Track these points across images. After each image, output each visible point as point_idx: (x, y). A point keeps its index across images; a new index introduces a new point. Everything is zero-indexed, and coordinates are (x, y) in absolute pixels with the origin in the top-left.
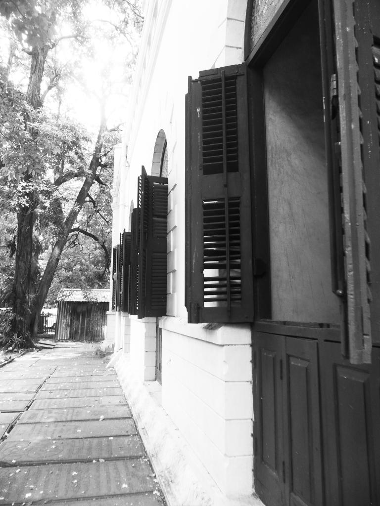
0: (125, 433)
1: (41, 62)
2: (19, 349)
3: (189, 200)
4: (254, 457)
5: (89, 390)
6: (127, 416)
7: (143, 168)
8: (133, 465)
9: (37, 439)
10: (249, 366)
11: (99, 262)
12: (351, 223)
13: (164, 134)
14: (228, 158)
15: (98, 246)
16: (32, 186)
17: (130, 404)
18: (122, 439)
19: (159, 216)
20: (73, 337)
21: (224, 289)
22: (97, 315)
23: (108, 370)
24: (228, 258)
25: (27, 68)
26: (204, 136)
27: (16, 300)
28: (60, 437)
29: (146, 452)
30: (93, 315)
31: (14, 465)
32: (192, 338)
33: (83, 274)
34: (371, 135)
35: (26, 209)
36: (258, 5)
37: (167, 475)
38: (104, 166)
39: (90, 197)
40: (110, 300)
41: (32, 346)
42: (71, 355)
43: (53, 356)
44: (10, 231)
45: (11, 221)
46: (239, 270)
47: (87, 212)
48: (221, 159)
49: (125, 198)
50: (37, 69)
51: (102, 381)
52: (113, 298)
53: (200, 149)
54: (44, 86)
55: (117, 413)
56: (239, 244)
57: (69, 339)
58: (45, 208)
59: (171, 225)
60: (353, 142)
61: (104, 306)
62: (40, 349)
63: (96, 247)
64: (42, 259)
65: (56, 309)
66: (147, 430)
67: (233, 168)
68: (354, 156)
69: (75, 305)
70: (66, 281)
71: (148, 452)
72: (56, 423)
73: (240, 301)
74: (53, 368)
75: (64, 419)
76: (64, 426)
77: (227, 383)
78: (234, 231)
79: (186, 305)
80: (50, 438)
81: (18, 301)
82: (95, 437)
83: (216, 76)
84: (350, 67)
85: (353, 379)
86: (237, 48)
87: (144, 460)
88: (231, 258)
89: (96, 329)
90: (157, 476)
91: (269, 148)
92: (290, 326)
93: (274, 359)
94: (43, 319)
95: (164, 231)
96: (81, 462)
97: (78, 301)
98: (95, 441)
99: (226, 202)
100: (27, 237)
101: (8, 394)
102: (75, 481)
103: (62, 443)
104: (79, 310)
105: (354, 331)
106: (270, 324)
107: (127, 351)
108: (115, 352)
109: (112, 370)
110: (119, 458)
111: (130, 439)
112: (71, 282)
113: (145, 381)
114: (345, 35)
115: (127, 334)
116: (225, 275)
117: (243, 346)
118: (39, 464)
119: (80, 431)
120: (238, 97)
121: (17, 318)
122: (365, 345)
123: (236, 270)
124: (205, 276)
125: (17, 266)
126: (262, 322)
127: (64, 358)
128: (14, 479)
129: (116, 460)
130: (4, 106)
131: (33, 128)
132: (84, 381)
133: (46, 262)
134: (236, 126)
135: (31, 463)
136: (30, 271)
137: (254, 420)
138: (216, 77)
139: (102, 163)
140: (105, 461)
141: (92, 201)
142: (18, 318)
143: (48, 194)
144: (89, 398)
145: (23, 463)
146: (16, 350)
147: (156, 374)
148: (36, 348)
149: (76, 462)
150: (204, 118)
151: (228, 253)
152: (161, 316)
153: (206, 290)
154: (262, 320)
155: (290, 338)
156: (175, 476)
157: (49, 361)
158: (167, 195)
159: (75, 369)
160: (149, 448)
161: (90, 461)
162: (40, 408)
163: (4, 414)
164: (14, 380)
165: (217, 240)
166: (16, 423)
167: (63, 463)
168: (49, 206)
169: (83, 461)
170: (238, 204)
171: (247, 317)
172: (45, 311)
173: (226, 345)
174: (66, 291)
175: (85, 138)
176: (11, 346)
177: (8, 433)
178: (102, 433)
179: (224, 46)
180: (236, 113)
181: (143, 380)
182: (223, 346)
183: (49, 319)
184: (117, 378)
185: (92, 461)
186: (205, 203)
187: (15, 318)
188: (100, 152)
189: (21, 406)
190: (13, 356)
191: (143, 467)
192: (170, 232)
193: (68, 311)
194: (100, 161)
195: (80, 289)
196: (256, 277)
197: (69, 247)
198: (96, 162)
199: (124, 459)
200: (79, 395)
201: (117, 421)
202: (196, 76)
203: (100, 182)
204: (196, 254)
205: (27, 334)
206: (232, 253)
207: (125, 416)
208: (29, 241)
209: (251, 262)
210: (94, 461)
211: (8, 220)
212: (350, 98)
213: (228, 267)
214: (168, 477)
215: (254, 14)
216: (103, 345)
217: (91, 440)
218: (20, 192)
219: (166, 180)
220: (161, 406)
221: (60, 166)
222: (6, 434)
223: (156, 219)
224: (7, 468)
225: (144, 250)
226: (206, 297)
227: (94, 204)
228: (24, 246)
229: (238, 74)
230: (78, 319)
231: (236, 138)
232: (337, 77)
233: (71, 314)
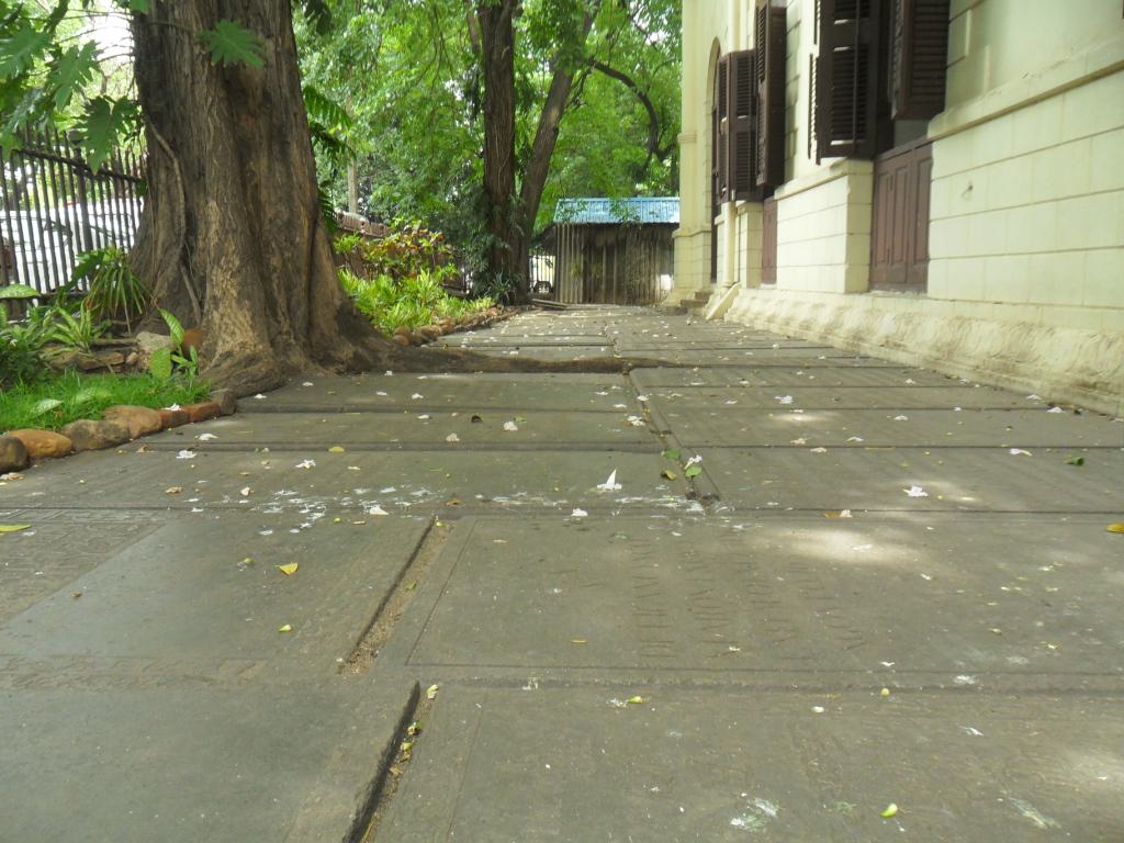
22: (638, 253)
27: (492, 207)
30: (630, 253)
69: (591, 234)
81: (497, 209)
104: (600, 241)
121: (497, 244)
124: (134, 207)
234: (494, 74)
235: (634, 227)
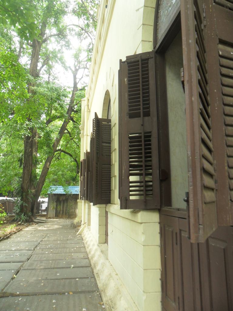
0: (86, 276)
1: (38, 51)
2: (25, 223)
3: (120, 134)
4: (161, 293)
5: (65, 249)
6: (88, 265)
7: (96, 113)
8: (90, 296)
9: (32, 279)
10: (158, 237)
11: (73, 170)
12: (192, 157)
13: (109, 92)
14: (144, 108)
15: (72, 160)
16: (31, 124)
17: (90, 258)
18: (84, 280)
19: (106, 143)
20: (57, 215)
21: (142, 188)
23: (78, 236)
24: (144, 169)
25: (30, 54)
26: (129, 95)
27: (23, 193)
28: (47, 278)
29: (98, 288)
30: (69, 202)
31: (18, 295)
32: (125, 218)
33: (63, 177)
34: (217, 98)
35: (28, 138)
36: (160, 16)
37: (110, 303)
38: (76, 112)
39: (68, 131)
40: (79, 193)
41: (32, 221)
42: (56, 227)
43: (45, 227)
44: (19, 152)
45: (20, 146)
46: (151, 177)
47: (66, 140)
48: (140, 109)
49: (88, 130)
50: (35, 57)
51: (73, 243)
52: (81, 192)
53: (127, 103)
54: (40, 65)
55: (82, 263)
56: (151, 161)
57: (55, 217)
58: (40, 137)
59: (112, 149)
60: (193, 108)
61: (75, 197)
62: (37, 223)
63: (71, 161)
64: (39, 169)
65: (48, 198)
66: (99, 274)
67: (147, 114)
68: (194, 117)
69: (59, 196)
70: (54, 181)
71: (99, 288)
72: (45, 269)
73: (152, 196)
74: (45, 235)
75: (50, 267)
76: (49, 271)
77: (145, 247)
78: (148, 151)
79: (119, 198)
80: (40, 279)
81: (24, 194)
82: (68, 279)
83: (136, 59)
84: (191, 63)
85: (218, 246)
86: (149, 42)
87: (97, 293)
88: (146, 169)
89: (71, 211)
90: (104, 304)
91: (169, 101)
92: (182, 212)
93: (172, 232)
94: (39, 204)
95: (109, 152)
96: (58, 294)
97: (60, 193)
98: (68, 281)
99: (143, 135)
100: (30, 155)
101: (16, 251)
102: (54, 306)
103: (48, 282)
104: (61, 199)
105: (193, 223)
106: (170, 210)
107: (89, 224)
108: (82, 225)
109: (80, 236)
110: (82, 292)
111: (89, 280)
112: (56, 182)
113: (99, 243)
114: (188, 45)
115: (89, 214)
116: (142, 180)
117: (154, 223)
118: (33, 295)
119: (59, 274)
120: (150, 71)
121: (23, 205)
122: (200, 231)
123: (149, 176)
125: (24, 173)
126: (165, 208)
127: (52, 228)
128: (18, 304)
129: (80, 293)
130: (15, 78)
131: (33, 90)
132: (63, 243)
133: (41, 170)
134: (148, 89)
135: (28, 294)
136: (31, 176)
137: (161, 270)
138: (137, 59)
139: (75, 110)
140: (73, 293)
141: (69, 133)
142: (24, 204)
143: (42, 129)
144: (65, 254)
145: (23, 294)
146: (23, 223)
147: (106, 240)
148: (35, 222)
149: (55, 294)
150: (129, 84)
151: (144, 166)
152: (108, 204)
153: (131, 189)
154: (165, 207)
155: (181, 219)
156: (115, 304)
157: (42, 230)
158: (111, 130)
159: (58, 236)
160: (100, 285)
161: (64, 293)
162: (36, 259)
163: (14, 263)
164: (21, 242)
165: (136, 159)
166: (21, 269)
167: (48, 294)
168: (43, 136)
169: (59, 293)
170: (150, 136)
171: (156, 206)
172: (40, 199)
173: (144, 223)
174: (53, 188)
175: (64, 95)
176: (20, 221)
177: (16, 275)
178: (72, 276)
179: (141, 41)
180: (148, 81)
181: (98, 243)
182: (141, 223)
183: (43, 205)
184: (83, 241)
185: (65, 294)
186: (130, 135)
187: (22, 204)
188: (73, 103)
189: (24, 258)
190: (21, 227)
191: (96, 298)
192: (112, 152)
193: (54, 200)
194: (73, 108)
195: (62, 186)
196: (161, 181)
197: (55, 161)
198: (71, 109)
199: (85, 293)
200: (59, 252)
201: (81, 269)
202: (124, 59)
203: (73, 121)
204: (125, 167)
205: (30, 214)
206: (146, 166)
207: (86, 265)
208: (31, 157)
209: (158, 171)
210: (66, 294)
211: (18, 145)
212: (191, 82)
213: (144, 174)
214: (110, 304)
215: (158, 21)
216: (76, 221)
217: (65, 280)
218: (25, 127)
219: (110, 121)
220: (108, 259)
221: (50, 112)
222: (15, 276)
223: (104, 144)
224: (14, 297)
225: (97, 164)
226: (131, 193)
227: (70, 135)
228: (28, 161)
229: (149, 57)
230: (60, 205)
231: (148, 96)
232: (183, 69)
233: (56, 202)
234: (26, 156)
235: (70, 195)
